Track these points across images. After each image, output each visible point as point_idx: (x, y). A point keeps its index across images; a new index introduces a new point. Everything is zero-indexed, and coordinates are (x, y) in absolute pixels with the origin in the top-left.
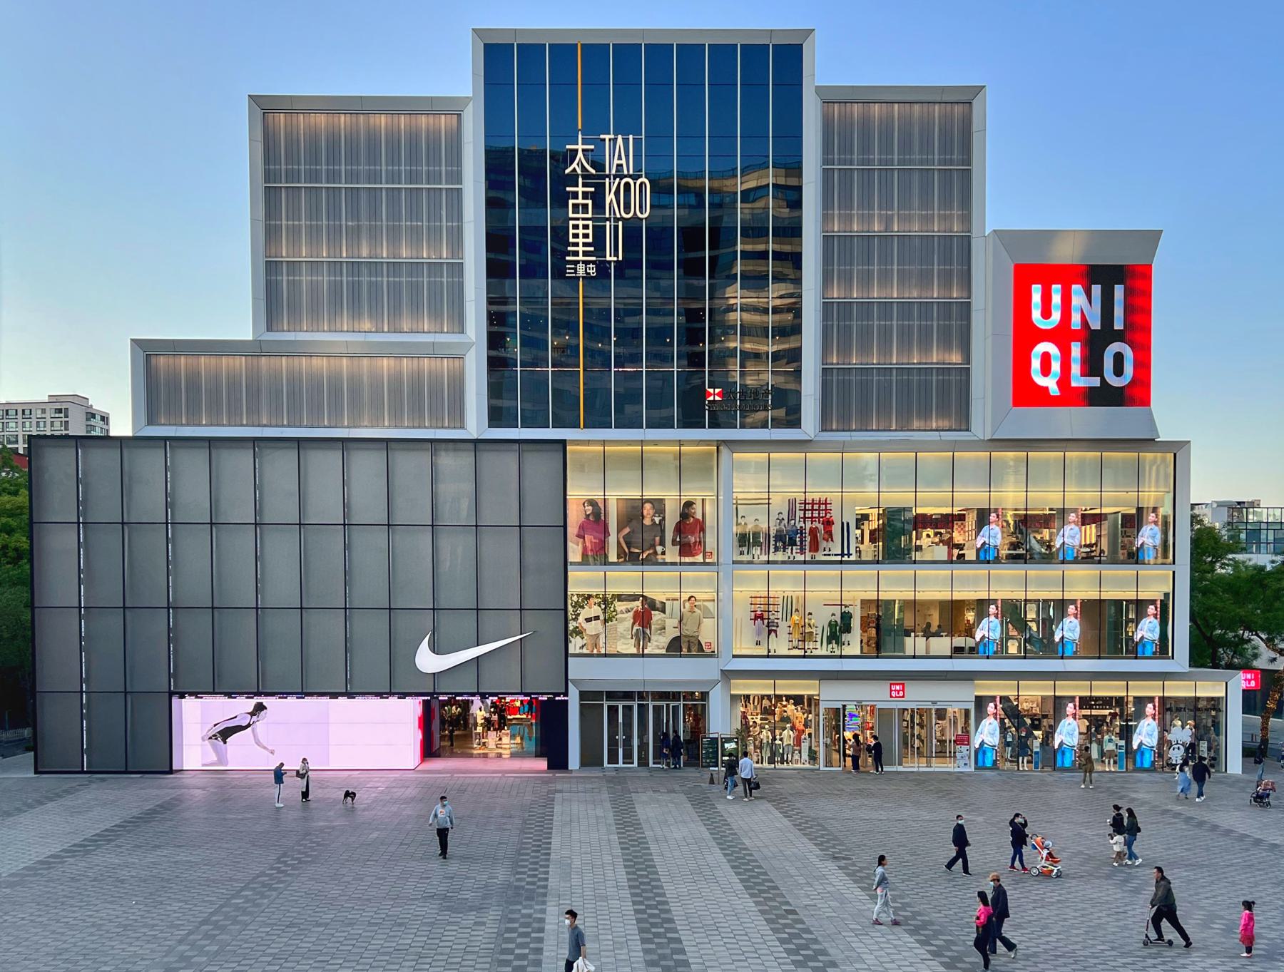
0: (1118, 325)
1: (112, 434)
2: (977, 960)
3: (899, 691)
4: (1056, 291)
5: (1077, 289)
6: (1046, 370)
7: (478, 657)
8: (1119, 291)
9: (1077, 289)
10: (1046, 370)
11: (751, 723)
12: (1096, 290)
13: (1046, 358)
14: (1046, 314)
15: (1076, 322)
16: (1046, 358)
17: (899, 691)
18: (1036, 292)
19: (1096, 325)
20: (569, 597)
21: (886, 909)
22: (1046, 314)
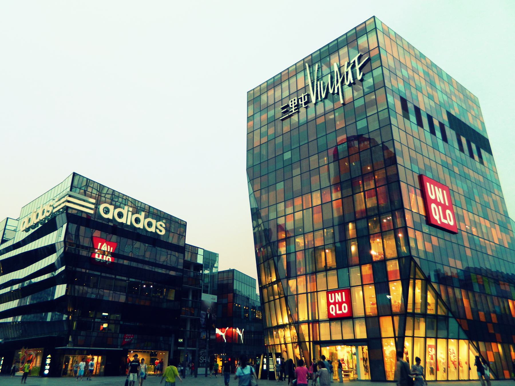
1: (407, 318)
3: (340, 304)
4: (333, 294)
5: (336, 294)
6: (332, 311)
7: (311, 54)
8: (343, 293)
10: (332, 311)
11: (329, 105)
12: (340, 293)
13: (332, 308)
14: (332, 299)
15: (337, 301)
16: (332, 308)
17: (340, 304)
18: (330, 295)
19: (340, 300)
21: (21, 373)
22: (332, 299)
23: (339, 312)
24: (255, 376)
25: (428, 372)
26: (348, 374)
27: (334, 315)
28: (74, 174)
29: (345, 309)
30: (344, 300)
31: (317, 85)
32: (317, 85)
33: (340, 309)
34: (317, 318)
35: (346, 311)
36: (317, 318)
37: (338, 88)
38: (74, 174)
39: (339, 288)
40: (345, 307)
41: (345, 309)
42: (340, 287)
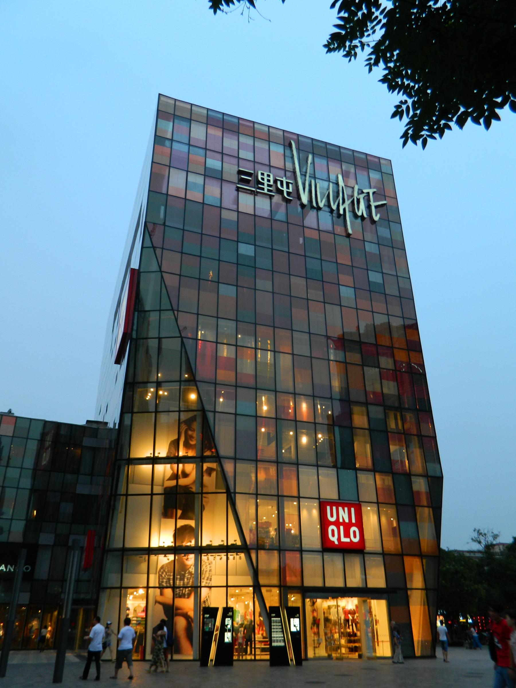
0: (354, 521)
2: (232, 391)
3: (347, 526)
4: (334, 508)
5: (340, 509)
6: (333, 535)
8: (353, 510)
9: (340, 509)
10: (333, 535)
13: (333, 531)
14: (332, 516)
15: (341, 520)
16: (333, 531)
19: (347, 521)
20: (175, 595)
22: (332, 516)
23: (344, 539)
24: (165, 638)
25: (353, 656)
26: (356, 647)
27: (336, 543)
28: (160, 94)
29: (355, 536)
30: (354, 521)
31: (310, 185)
32: (310, 185)
33: (347, 535)
34: (200, 545)
35: (356, 540)
36: (200, 545)
37: (344, 210)
38: (160, 94)
39: (339, 499)
40: (354, 532)
41: (355, 536)
42: (341, 498)
